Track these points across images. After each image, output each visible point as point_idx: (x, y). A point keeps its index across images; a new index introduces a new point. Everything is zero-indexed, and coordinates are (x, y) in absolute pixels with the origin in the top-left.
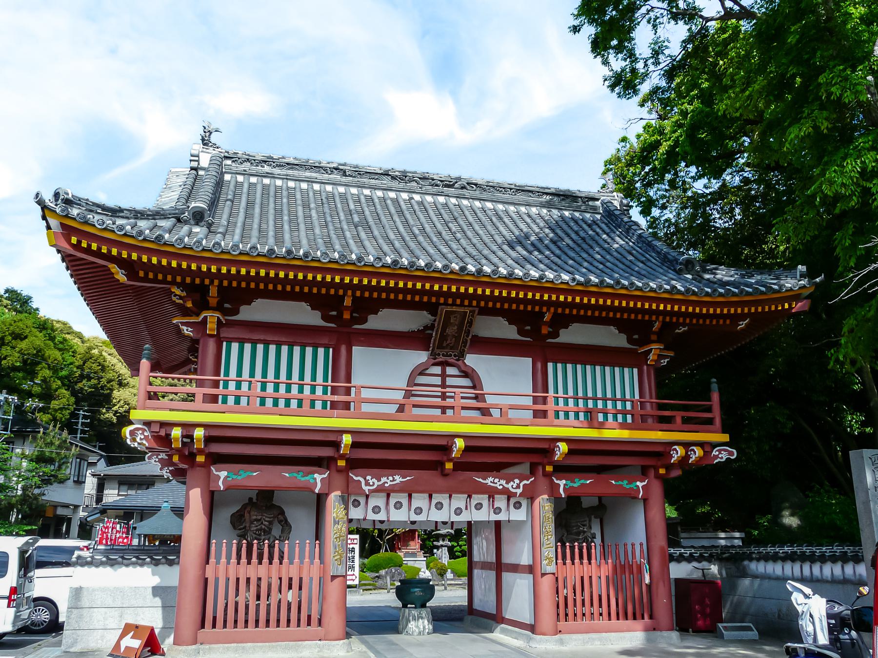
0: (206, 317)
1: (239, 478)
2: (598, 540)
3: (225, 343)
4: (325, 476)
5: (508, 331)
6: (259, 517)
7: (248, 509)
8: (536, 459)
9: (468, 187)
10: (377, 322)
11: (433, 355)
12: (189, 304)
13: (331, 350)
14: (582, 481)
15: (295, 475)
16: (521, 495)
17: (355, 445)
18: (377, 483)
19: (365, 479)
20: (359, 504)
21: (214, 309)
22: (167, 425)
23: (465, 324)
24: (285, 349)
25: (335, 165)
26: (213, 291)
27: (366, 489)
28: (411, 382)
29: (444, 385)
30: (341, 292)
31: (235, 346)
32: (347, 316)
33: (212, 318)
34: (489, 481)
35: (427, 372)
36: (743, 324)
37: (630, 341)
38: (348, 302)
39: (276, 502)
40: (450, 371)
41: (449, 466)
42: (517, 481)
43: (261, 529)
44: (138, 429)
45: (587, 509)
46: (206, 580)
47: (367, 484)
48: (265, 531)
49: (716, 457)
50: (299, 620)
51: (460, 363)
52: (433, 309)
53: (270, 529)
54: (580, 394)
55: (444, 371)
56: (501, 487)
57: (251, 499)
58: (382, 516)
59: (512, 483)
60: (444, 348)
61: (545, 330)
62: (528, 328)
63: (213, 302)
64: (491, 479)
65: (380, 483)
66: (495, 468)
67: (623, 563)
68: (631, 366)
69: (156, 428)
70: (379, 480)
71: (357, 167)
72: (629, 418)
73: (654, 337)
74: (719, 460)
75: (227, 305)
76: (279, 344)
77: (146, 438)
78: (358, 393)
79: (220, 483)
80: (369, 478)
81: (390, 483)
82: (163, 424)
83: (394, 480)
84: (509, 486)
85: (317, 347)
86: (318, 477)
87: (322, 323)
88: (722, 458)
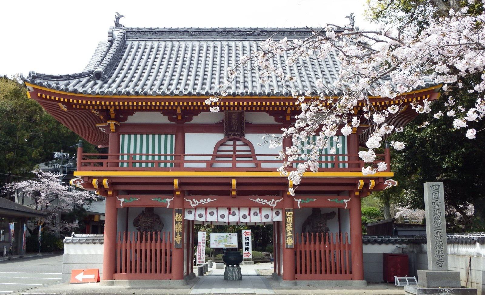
1: (130, 201)
3: (121, 135)
4: (172, 200)
6: (146, 220)
7: (141, 216)
9: (262, 34)
11: (227, 135)
12: (102, 117)
13: (174, 136)
14: (311, 200)
15: (157, 199)
17: (237, 184)
19: (192, 201)
20: (214, 213)
22: (91, 178)
24: (151, 136)
25: (185, 30)
27: (193, 205)
28: (216, 149)
29: (235, 151)
31: (126, 137)
34: (258, 200)
35: (227, 144)
40: (238, 143)
42: (273, 200)
43: (147, 226)
45: (324, 214)
47: (193, 203)
48: (149, 227)
49: (387, 185)
51: (242, 139)
54: (150, 152)
55: (235, 143)
56: (264, 204)
57: (143, 212)
58: (225, 220)
59: (270, 201)
60: (232, 131)
63: (113, 116)
64: (259, 199)
65: (199, 203)
67: (349, 243)
72: (329, 165)
74: (388, 187)
76: (148, 135)
77: (82, 184)
79: (121, 205)
80: (194, 200)
81: (205, 202)
83: (207, 201)
84: (269, 203)
85: (130, 134)
86: (346, 201)
87: (169, 122)
88: (389, 186)
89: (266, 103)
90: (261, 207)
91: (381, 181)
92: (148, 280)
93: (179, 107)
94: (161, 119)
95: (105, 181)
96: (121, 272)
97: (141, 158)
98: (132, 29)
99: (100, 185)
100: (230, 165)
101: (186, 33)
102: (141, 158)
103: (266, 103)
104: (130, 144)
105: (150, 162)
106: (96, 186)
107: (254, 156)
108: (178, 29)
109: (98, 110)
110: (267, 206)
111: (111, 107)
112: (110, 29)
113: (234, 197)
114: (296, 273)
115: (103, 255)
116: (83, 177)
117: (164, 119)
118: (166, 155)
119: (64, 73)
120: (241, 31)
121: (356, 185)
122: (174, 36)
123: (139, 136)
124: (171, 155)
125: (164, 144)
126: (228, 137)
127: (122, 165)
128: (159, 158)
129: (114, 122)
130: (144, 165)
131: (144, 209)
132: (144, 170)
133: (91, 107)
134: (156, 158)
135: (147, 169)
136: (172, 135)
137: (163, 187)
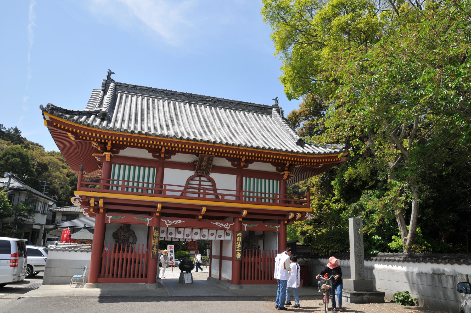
0: (106, 155)
2: (261, 248)
5: (228, 164)
8: (236, 215)
10: (174, 158)
12: (99, 149)
16: (229, 229)
17: (163, 207)
18: (171, 223)
20: (213, 234)
21: (109, 151)
23: (210, 160)
26: (109, 144)
27: (167, 225)
28: (188, 183)
30: (160, 147)
31: (117, 166)
32: (162, 156)
33: (108, 155)
34: (216, 224)
36: (321, 166)
37: (277, 169)
38: (163, 150)
39: (131, 228)
40: (203, 179)
41: (200, 217)
42: (228, 224)
44: (77, 198)
45: (257, 236)
46: (102, 258)
47: (168, 223)
49: (307, 217)
50: (138, 275)
52: (197, 155)
53: (129, 239)
55: (200, 179)
57: (121, 227)
60: (201, 170)
61: (242, 164)
62: (236, 163)
64: (217, 223)
66: (222, 219)
68: (277, 180)
69: (84, 198)
70: (172, 222)
71: (171, 91)
72: (271, 201)
73: (286, 169)
75: (114, 149)
78: (165, 187)
79: (109, 220)
80: (168, 220)
82: (87, 197)
84: (224, 226)
86: (148, 219)
89: (226, 151)
90: (217, 228)
91: (303, 214)
92: (135, 284)
93: (163, 147)
94: (145, 154)
95: (101, 201)
96: (108, 276)
97: (138, 185)
98: (121, 84)
99: (97, 205)
100: (196, 196)
101: (162, 93)
102: (138, 185)
103: (226, 151)
104: (120, 172)
105: (140, 188)
106: (92, 205)
107: (215, 189)
108: (156, 89)
109: (97, 142)
110: (222, 228)
111: (109, 141)
112: (104, 81)
113: (200, 220)
114: (241, 279)
115: (90, 262)
116: (81, 196)
117: (149, 156)
118: (148, 183)
119: (70, 109)
120: (203, 98)
121: (199, 210)
122: (153, 94)
123: (122, 166)
124: (153, 184)
125: (148, 175)
126: (197, 175)
127: (112, 188)
128: (148, 186)
129: (110, 153)
130: (130, 190)
131: (122, 225)
132: (129, 194)
133: (92, 139)
134: (145, 185)
135: (137, 194)
136: (154, 168)
137: (146, 209)
